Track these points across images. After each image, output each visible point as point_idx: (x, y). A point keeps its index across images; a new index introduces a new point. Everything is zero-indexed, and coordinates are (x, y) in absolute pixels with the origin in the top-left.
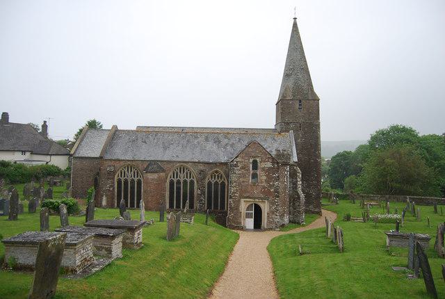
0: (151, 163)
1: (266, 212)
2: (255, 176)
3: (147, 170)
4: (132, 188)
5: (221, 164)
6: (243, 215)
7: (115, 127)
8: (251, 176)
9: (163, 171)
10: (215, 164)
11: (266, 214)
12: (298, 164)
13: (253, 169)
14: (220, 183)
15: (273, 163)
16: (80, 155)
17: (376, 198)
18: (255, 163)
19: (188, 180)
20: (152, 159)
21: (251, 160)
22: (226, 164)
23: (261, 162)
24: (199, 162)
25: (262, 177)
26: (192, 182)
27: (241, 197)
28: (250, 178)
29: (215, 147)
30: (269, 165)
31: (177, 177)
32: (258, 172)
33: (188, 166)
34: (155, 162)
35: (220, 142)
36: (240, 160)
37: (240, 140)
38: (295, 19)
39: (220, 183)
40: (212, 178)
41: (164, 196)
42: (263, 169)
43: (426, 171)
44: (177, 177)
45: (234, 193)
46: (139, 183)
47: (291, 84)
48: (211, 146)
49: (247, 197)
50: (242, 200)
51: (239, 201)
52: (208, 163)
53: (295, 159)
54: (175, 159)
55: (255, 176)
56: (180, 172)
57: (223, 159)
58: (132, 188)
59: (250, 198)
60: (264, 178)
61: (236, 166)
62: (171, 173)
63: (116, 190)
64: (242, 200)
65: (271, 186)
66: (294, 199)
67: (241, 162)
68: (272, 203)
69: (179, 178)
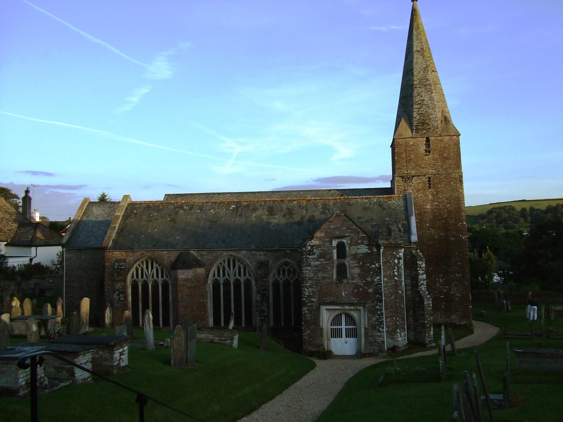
2: (342, 271)
4: (227, 293)
8: (335, 269)
12: (420, 243)
14: (292, 282)
15: (370, 245)
21: (335, 243)
25: (353, 270)
26: (248, 283)
30: (363, 249)
32: (348, 262)
40: (279, 274)
41: (204, 307)
42: (355, 256)
43: (6, 261)
44: (142, 276)
45: (309, 296)
50: (323, 308)
51: (318, 309)
55: (342, 271)
58: (227, 293)
59: (337, 304)
60: (357, 271)
61: (311, 253)
62: (214, 269)
63: (130, 299)
64: (323, 308)
67: (318, 246)
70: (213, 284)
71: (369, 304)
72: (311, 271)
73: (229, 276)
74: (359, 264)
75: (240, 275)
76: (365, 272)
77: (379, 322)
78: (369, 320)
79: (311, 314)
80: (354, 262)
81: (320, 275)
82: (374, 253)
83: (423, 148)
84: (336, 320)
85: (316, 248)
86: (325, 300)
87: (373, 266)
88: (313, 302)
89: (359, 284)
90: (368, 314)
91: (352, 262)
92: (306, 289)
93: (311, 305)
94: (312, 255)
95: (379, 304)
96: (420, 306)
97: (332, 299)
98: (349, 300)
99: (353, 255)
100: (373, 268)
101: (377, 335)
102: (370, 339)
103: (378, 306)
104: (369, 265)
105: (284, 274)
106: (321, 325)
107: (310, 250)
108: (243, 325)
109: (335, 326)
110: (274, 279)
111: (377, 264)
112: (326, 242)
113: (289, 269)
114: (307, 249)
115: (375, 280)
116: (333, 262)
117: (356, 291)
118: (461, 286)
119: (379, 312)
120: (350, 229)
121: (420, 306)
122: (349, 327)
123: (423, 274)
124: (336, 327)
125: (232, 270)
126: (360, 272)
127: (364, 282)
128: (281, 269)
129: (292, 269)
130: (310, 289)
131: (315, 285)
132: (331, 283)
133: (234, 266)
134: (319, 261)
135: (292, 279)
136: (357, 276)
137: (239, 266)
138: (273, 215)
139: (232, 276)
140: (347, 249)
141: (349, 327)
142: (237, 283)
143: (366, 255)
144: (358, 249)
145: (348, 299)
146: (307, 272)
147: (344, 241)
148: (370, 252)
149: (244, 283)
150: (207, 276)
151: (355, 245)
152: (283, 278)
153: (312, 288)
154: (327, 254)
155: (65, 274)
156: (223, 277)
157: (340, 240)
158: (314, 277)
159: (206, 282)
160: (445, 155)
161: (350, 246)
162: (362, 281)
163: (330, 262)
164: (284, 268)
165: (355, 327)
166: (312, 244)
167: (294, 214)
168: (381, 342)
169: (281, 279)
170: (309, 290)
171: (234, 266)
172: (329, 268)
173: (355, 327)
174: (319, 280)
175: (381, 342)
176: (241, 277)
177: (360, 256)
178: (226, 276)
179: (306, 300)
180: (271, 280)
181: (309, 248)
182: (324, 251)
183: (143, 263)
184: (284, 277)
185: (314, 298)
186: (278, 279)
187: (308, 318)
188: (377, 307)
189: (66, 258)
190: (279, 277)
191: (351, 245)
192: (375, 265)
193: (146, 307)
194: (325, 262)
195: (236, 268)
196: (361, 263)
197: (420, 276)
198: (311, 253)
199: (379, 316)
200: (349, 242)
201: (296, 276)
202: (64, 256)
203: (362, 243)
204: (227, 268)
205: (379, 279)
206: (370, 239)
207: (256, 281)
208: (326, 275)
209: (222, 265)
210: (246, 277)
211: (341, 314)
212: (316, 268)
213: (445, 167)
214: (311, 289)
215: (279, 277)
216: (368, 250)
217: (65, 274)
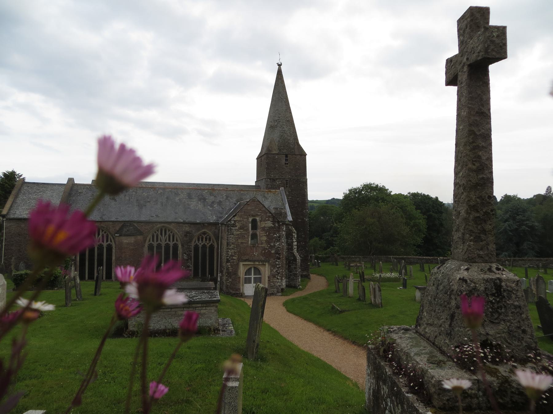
0: (125, 224)
1: (267, 276)
2: (254, 236)
3: (120, 232)
4: (100, 255)
5: (210, 224)
6: (242, 280)
7: (71, 180)
8: (250, 237)
9: (141, 233)
10: (202, 225)
11: (267, 278)
12: (294, 223)
13: (252, 229)
14: (208, 246)
15: (274, 222)
16: (16, 216)
17: (358, 259)
18: (254, 222)
19: (171, 244)
20: (127, 219)
21: (250, 219)
22: (215, 224)
23: (261, 221)
24: (184, 223)
26: (175, 247)
27: (240, 260)
28: (250, 239)
29: (200, 206)
30: (269, 224)
31: (157, 241)
32: (258, 232)
33: (171, 227)
34: (131, 223)
35: (205, 199)
36: (239, 219)
37: (227, 197)
38: (280, 65)
39: (200, 246)
40: (199, 240)
42: (263, 229)
45: (232, 256)
46: (109, 248)
47: (276, 136)
48: (194, 204)
49: (245, 261)
50: (241, 264)
51: (238, 265)
52: (195, 224)
53: (290, 218)
54: (155, 219)
55: (254, 236)
56: (161, 234)
57: (212, 219)
58: (100, 255)
60: (265, 238)
61: (234, 225)
62: (150, 236)
64: (241, 264)
65: (271, 247)
66: (291, 261)
67: (240, 221)
68: (273, 266)
69: (159, 242)
70: (148, 247)
71: (272, 261)
72: (234, 238)
73: (161, 241)
74: (266, 233)
75: (169, 241)
76: (270, 239)
77: (278, 272)
78: (271, 271)
79: (233, 267)
80: (263, 232)
81: (240, 241)
82: (276, 227)
83: (283, 161)
84: (248, 272)
85: (238, 222)
86: (242, 258)
87: (275, 235)
88: (234, 259)
89: (265, 247)
90: (271, 268)
91: (261, 232)
92: (229, 251)
93: (233, 262)
94: (235, 227)
95: (278, 261)
96: (294, 262)
97: (247, 257)
98: (259, 258)
99: (262, 228)
100: (275, 236)
101: (276, 282)
102: (271, 284)
103: (277, 262)
104: (272, 234)
105: (202, 240)
106: (239, 275)
107: (233, 224)
108: (200, 276)
109: (250, 277)
110: (195, 244)
111: (278, 234)
112: (245, 218)
113: (206, 237)
114: (232, 223)
115: (276, 245)
116: (249, 233)
117: (263, 252)
118: (304, 250)
119: (278, 266)
120: (261, 210)
121: (294, 262)
122: (256, 276)
123: (295, 242)
124: (257, 276)
125: (163, 237)
126: (267, 239)
127: (269, 246)
128: (201, 237)
129: (208, 237)
130: (233, 250)
131: (236, 248)
132: (247, 247)
133: (165, 234)
134: (240, 231)
135: (208, 244)
136: (264, 242)
137: (103, 234)
138: (192, 199)
139: (163, 241)
140: (259, 224)
141: (256, 276)
142: (167, 246)
143: (270, 228)
144: (266, 224)
145: (258, 257)
146: (231, 238)
147: (257, 218)
148: (273, 226)
149: (173, 246)
150: (145, 241)
151: (264, 221)
152: (201, 243)
153: (234, 250)
154: (245, 227)
155: (4, 239)
156: (157, 242)
157: (254, 218)
158: (235, 242)
159: (143, 246)
160: (297, 166)
161: (261, 222)
162: (268, 245)
163: (247, 232)
164: (202, 236)
165: (260, 276)
166: (235, 220)
167: (207, 199)
168: (279, 286)
169: (200, 244)
170: (231, 251)
171: (165, 234)
172: (246, 236)
173: (260, 276)
174: (239, 245)
175: (279, 286)
176: (154, 242)
177: (267, 228)
178: (159, 242)
179: (229, 258)
180: (193, 244)
181: (233, 222)
182: (243, 225)
183: (158, 231)
184: (202, 242)
185: (235, 256)
186: (198, 244)
187: (230, 271)
188: (276, 263)
189: (6, 226)
190: (199, 242)
191: (261, 221)
192: (276, 234)
193: (100, 264)
194: (244, 232)
195: (100, 236)
196: (267, 234)
197: (294, 243)
198: (234, 225)
199: (278, 269)
200: (260, 219)
201: (211, 242)
202: (5, 224)
203: (269, 220)
204: (160, 236)
205: (278, 244)
206: (274, 217)
207: (183, 245)
208: (243, 241)
209: (156, 233)
210: (108, 243)
211: (251, 268)
212: (237, 236)
213: (296, 174)
214: (233, 251)
215: (199, 242)
216: (272, 225)
217: (4, 239)
